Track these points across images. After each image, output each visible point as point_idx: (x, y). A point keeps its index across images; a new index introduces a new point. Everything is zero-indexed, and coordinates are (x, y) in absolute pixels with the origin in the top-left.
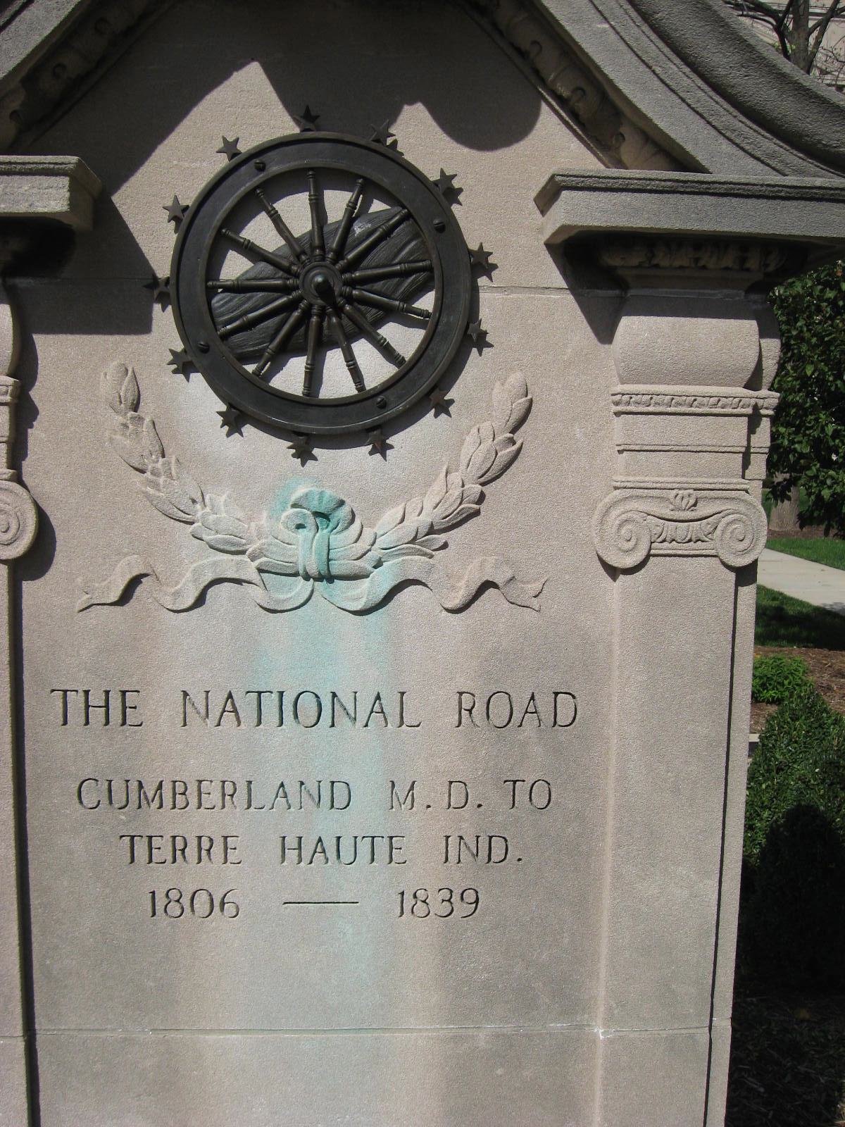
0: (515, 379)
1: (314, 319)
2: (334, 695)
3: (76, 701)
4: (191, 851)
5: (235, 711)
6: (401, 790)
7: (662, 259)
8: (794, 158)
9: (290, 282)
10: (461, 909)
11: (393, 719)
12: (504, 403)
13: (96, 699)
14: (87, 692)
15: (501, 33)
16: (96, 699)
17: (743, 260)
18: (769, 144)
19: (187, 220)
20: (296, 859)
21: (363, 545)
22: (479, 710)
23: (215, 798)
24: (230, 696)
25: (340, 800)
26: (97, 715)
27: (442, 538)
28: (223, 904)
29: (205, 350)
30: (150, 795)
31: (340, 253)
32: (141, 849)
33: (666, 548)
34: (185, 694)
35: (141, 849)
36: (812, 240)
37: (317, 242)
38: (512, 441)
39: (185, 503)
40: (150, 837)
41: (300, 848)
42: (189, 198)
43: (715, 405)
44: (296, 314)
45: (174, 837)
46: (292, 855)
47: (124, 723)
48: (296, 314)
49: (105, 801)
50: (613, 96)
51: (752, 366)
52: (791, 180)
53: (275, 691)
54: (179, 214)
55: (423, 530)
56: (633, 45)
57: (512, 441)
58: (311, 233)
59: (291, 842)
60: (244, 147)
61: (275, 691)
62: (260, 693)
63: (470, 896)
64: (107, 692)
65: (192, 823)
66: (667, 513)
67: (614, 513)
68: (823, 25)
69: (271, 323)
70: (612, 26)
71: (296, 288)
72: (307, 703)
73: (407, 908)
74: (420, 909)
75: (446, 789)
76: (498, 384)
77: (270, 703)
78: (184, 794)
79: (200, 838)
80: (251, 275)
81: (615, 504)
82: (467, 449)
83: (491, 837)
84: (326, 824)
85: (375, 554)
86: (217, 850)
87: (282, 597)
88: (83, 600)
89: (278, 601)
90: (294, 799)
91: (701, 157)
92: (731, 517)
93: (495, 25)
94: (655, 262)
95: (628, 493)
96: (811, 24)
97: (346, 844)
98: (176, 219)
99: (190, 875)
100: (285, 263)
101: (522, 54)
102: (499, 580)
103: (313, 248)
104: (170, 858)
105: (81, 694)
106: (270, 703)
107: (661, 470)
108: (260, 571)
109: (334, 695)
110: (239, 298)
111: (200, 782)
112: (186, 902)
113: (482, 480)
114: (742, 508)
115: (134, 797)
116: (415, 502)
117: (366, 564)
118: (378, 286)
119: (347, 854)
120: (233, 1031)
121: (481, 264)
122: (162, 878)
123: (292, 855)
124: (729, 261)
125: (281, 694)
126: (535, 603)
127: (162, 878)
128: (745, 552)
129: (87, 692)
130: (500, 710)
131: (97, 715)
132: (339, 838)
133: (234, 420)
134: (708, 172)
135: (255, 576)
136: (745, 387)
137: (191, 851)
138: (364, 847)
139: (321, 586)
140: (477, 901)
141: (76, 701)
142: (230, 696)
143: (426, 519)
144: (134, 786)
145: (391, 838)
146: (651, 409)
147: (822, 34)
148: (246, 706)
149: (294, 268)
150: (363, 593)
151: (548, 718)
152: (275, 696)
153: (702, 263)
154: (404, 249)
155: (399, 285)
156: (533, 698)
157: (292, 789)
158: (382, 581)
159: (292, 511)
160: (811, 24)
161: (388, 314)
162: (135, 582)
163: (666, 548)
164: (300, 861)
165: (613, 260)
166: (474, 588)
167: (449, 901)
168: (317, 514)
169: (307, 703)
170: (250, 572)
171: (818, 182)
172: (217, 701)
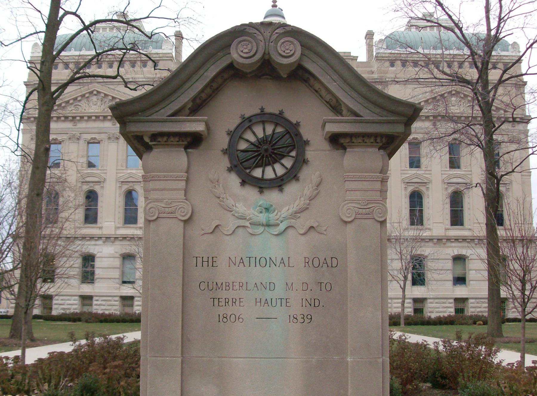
0: (317, 173)
1: (264, 159)
2: (270, 258)
3: (199, 260)
4: (230, 303)
5: (243, 262)
6: (290, 285)
7: (354, 140)
8: (385, 113)
9: (259, 146)
10: (307, 321)
11: (287, 264)
12: (315, 178)
13: (205, 259)
14: (203, 257)
15: (311, 87)
16: (205, 259)
17: (376, 140)
18: (378, 110)
19: (231, 134)
20: (260, 305)
21: (278, 217)
22: (310, 263)
23: (237, 287)
24: (242, 259)
25: (272, 288)
26: (205, 264)
27: (299, 215)
28: (239, 318)
29: (236, 166)
30: (219, 286)
31: (270, 142)
32: (216, 301)
33: (359, 216)
34: (230, 258)
35: (216, 301)
36: (394, 134)
37: (265, 139)
38: (317, 189)
39: (230, 206)
40: (219, 299)
41: (261, 302)
42: (232, 128)
43: (371, 178)
44: (260, 157)
45: (225, 299)
46: (258, 304)
47: (213, 266)
48: (260, 157)
49: (207, 288)
50: (339, 100)
51: (381, 168)
52: (385, 118)
53: (254, 257)
54: (230, 133)
55: (294, 213)
56: (342, 87)
57: (317, 189)
58: (263, 137)
59: (258, 300)
60: (247, 116)
61: (254, 257)
62: (250, 258)
63: (309, 317)
64: (208, 258)
65: (231, 294)
66: (360, 207)
67: (345, 207)
68: (496, 87)
69: (253, 160)
70: (338, 84)
71: (260, 148)
72: (263, 261)
73: (291, 321)
74: (295, 320)
75: (302, 285)
76: (313, 175)
77: (253, 260)
78: (228, 286)
79: (233, 299)
80: (249, 147)
81: (345, 204)
82: (305, 192)
83: (315, 299)
84: (268, 295)
85: (281, 219)
86: (238, 302)
87: (256, 231)
88: (203, 232)
89: (255, 232)
90: (259, 287)
91: (361, 114)
92: (376, 208)
93: (309, 85)
94: (353, 141)
95: (349, 202)
96: (490, 88)
97: (274, 301)
98: (228, 134)
99: (229, 310)
100: (257, 145)
101: (317, 91)
102: (314, 226)
103: (264, 141)
104: (224, 305)
105: (201, 258)
106: (253, 260)
107: (358, 195)
108: (250, 224)
109: (270, 258)
110: (244, 154)
111: (233, 283)
112: (228, 318)
113: (310, 199)
114: (381, 205)
115: (215, 286)
116: (292, 206)
117: (278, 222)
118: (281, 150)
119: (274, 304)
120: (241, 358)
121: (307, 143)
122: (222, 311)
123: (258, 304)
124: (372, 140)
125: (256, 258)
126: (325, 233)
127: (222, 311)
128: (381, 217)
129: (203, 257)
130: (316, 263)
131: (205, 264)
132: (272, 299)
133: (243, 183)
134: (362, 117)
135: (249, 225)
136: (380, 173)
137: (230, 303)
138: (279, 301)
139: (267, 228)
140: (311, 318)
141: (199, 260)
142: (242, 259)
143: (295, 209)
144: (215, 283)
145: (286, 299)
146: (354, 179)
147: (495, 92)
148: (246, 261)
149: (261, 143)
150: (276, 231)
151: (330, 265)
152: (254, 259)
153: (365, 141)
154: (287, 140)
155: (286, 149)
156: (325, 259)
157: (259, 285)
158: (282, 227)
159: (258, 208)
160: (490, 88)
161: (283, 157)
162: (217, 227)
163: (359, 216)
164: (261, 306)
165: (342, 141)
166: (308, 228)
167: (303, 318)
168: (266, 209)
169: (263, 261)
170: (247, 224)
171: (392, 118)
172: (238, 260)
